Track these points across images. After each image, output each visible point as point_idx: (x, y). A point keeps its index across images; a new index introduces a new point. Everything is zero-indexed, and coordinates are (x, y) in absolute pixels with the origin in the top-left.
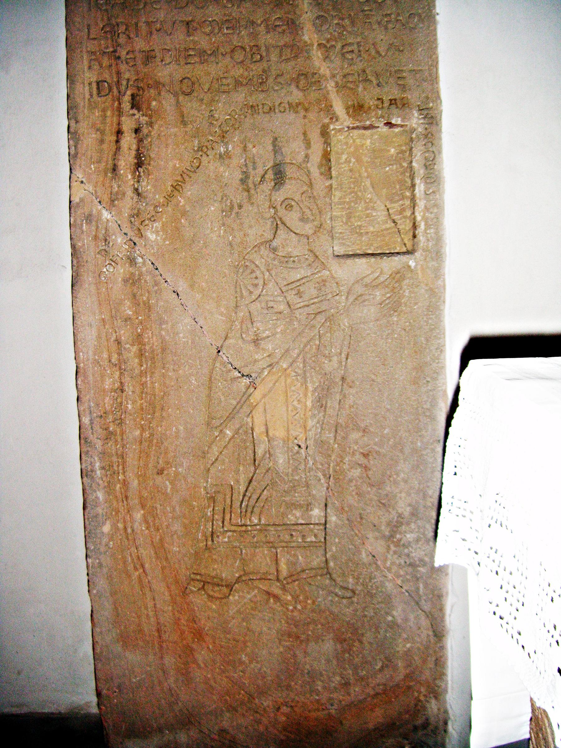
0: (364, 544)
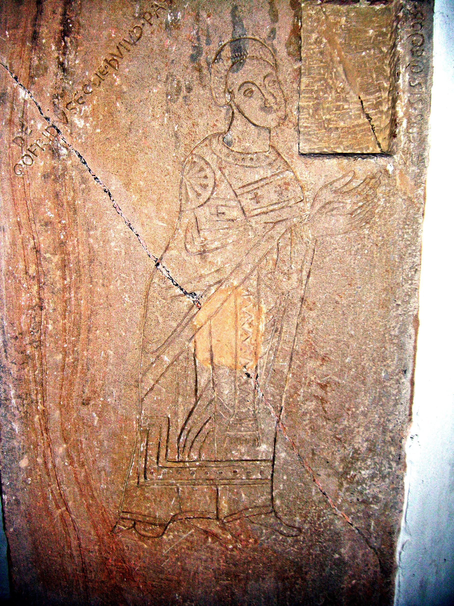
0: (314, 480)
